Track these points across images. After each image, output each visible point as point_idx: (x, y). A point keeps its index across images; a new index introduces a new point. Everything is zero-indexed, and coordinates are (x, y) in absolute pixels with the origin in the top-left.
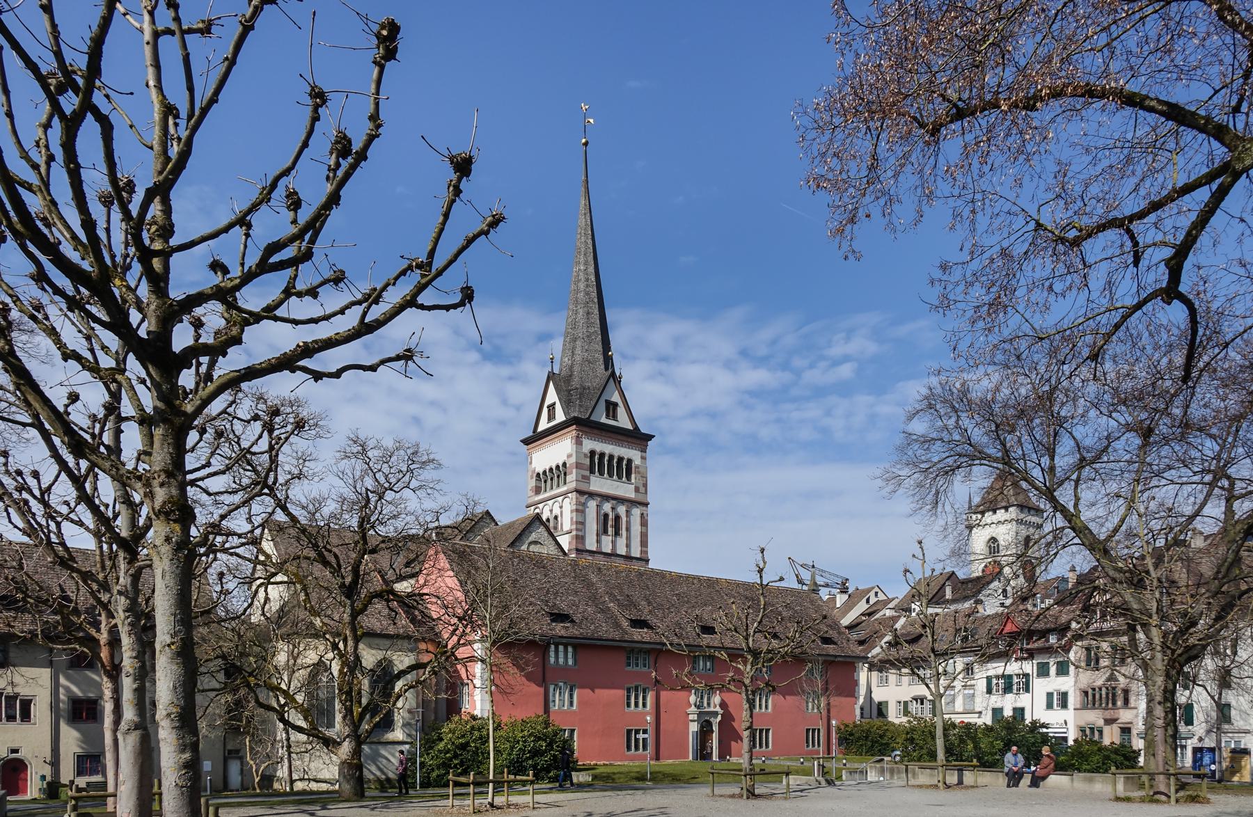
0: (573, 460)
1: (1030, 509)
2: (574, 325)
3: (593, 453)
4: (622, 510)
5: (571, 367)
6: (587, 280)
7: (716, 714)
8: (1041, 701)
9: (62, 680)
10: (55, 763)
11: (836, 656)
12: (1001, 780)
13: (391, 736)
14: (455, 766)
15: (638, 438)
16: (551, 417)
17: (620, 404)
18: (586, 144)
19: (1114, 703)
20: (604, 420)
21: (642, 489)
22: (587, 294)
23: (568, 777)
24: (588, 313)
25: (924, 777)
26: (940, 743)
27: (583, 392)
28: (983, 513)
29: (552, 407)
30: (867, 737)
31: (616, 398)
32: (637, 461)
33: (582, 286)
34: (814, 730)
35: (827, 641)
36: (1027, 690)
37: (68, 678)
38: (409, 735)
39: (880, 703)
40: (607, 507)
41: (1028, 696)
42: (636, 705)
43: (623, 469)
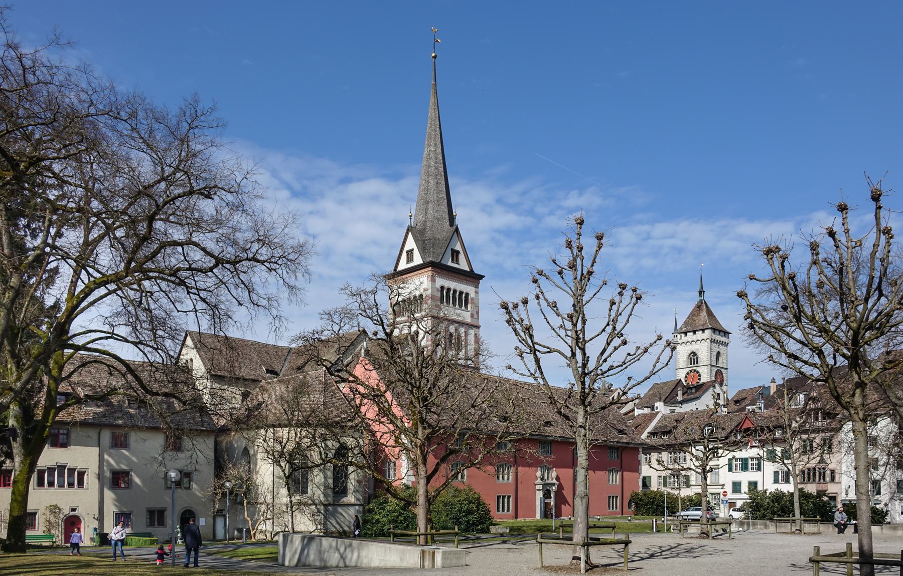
0: (429, 292)
1: (720, 331)
2: (427, 191)
3: (442, 288)
4: (462, 330)
5: (425, 222)
6: (436, 158)
7: (554, 484)
8: (770, 477)
9: (106, 457)
10: (100, 519)
11: (629, 444)
12: (831, 529)
13: (345, 500)
14: (401, 522)
15: (473, 278)
16: (410, 258)
17: (461, 252)
18: (435, 57)
19: (824, 479)
20: (450, 264)
21: (476, 316)
22: (437, 169)
23: (487, 531)
24: (437, 183)
25: (787, 527)
26: (420, 512)
27: (435, 242)
28: (686, 333)
29: (410, 252)
30: (653, 503)
31: (458, 247)
32: (472, 295)
33: (432, 162)
34: (504, 497)
35: (621, 432)
36: (759, 469)
37: (110, 455)
38: (358, 499)
39: (644, 478)
40: (452, 329)
41: (760, 473)
42: (503, 479)
43: (463, 300)
